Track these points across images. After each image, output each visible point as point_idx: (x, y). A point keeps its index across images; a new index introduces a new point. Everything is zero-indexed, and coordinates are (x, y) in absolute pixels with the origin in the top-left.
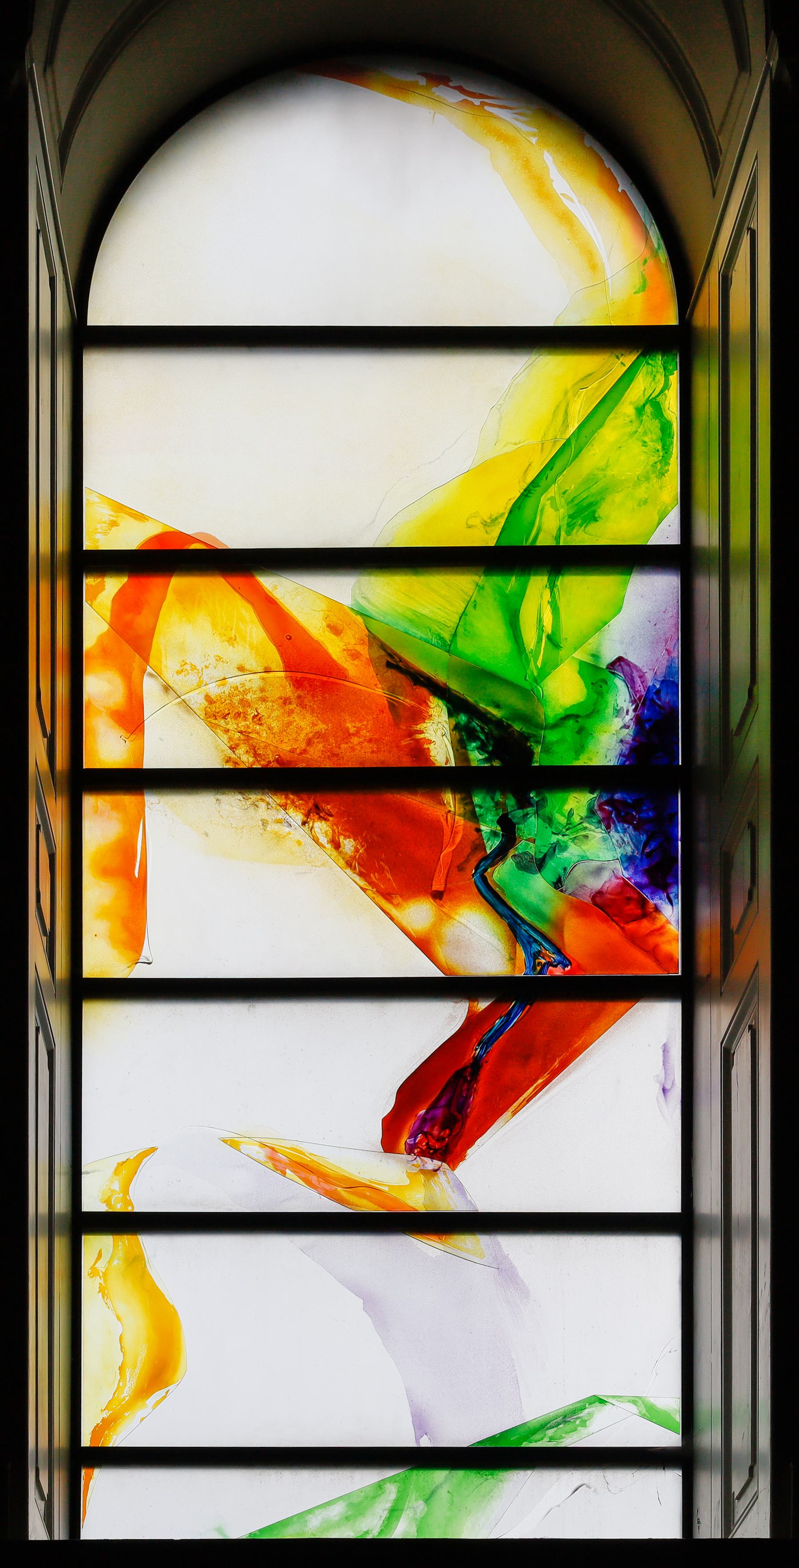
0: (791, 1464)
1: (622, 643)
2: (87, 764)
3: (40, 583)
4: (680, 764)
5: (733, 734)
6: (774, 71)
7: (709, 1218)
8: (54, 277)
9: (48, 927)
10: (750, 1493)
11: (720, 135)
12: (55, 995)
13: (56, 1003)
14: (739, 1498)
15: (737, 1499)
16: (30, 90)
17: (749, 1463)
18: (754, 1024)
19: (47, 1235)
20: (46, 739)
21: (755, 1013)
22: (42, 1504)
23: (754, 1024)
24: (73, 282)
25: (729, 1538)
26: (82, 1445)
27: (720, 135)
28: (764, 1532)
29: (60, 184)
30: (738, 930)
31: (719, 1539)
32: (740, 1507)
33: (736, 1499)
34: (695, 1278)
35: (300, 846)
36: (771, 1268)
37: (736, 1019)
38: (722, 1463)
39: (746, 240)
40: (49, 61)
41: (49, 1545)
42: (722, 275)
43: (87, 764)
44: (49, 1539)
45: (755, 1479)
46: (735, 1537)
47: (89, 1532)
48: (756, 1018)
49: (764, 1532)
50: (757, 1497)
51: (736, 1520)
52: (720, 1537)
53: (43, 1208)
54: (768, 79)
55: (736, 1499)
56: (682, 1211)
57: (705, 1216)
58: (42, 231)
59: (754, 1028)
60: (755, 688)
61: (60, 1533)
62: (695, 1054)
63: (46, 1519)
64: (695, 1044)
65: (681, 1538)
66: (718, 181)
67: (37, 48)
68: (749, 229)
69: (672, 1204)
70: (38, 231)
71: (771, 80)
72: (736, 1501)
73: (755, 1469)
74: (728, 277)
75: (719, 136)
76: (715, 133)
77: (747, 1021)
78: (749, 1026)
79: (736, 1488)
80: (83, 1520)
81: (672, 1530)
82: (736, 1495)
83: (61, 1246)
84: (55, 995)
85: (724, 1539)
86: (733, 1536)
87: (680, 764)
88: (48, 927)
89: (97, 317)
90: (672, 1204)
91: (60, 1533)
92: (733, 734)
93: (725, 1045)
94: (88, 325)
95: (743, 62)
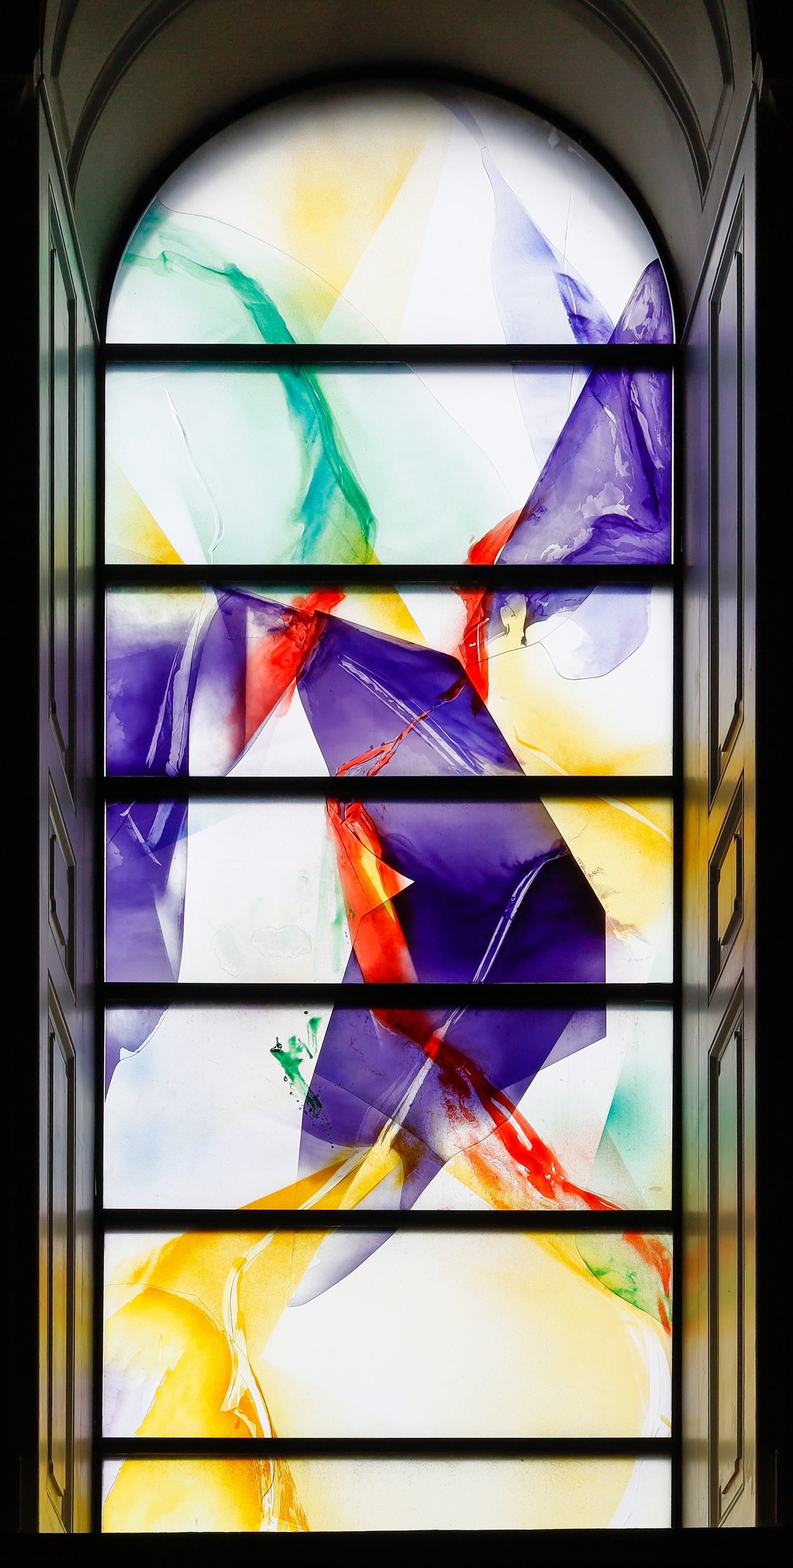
0: (776, 1450)
2: (106, 1434)
4: (672, 563)
5: (721, 943)
8: (74, 300)
11: (710, 150)
12: (76, 813)
13: (77, 1012)
18: (739, 1030)
25: (719, 1527)
27: (710, 150)
28: (751, 1523)
30: (726, 748)
31: (707, 1528)
32: (726, 1502)
34: (683, 1110)
35: (312, 1058)
36: (756, 645)
37: (724, 1024)
38: (709, 562)
39: (733, 845)
43: (106, 1434)
44: (66, 1532)
46: (722, 1527)
47: (112, 1524)
48: (742, 1026)
49: (751, 1523)
50: (743, 1489)
51: (723, 1510)
52: (708, 1527)
53: (59, 1433)
58: (57, 249)
61: (80, 1525)
63: (67, 967)
64: (683, 970)
65: (671, 1528)
66: (706, 199)
68: (736, 836)
74: (717, 867)
75: (709, 152)
76: (705, 147)
77: (734, 1027)
78: (735, 1032)
79: (723, 1481)
80: (106, 1094)
81: (664, 1522)
83: (82, 1245)
84: (76, 813)
85: (711, 1528)
87: (672, 563)
89: (114, 336)
90: (664, 1203)
92: (721, 943)
93: (711, 1054)
95: (728, 76)
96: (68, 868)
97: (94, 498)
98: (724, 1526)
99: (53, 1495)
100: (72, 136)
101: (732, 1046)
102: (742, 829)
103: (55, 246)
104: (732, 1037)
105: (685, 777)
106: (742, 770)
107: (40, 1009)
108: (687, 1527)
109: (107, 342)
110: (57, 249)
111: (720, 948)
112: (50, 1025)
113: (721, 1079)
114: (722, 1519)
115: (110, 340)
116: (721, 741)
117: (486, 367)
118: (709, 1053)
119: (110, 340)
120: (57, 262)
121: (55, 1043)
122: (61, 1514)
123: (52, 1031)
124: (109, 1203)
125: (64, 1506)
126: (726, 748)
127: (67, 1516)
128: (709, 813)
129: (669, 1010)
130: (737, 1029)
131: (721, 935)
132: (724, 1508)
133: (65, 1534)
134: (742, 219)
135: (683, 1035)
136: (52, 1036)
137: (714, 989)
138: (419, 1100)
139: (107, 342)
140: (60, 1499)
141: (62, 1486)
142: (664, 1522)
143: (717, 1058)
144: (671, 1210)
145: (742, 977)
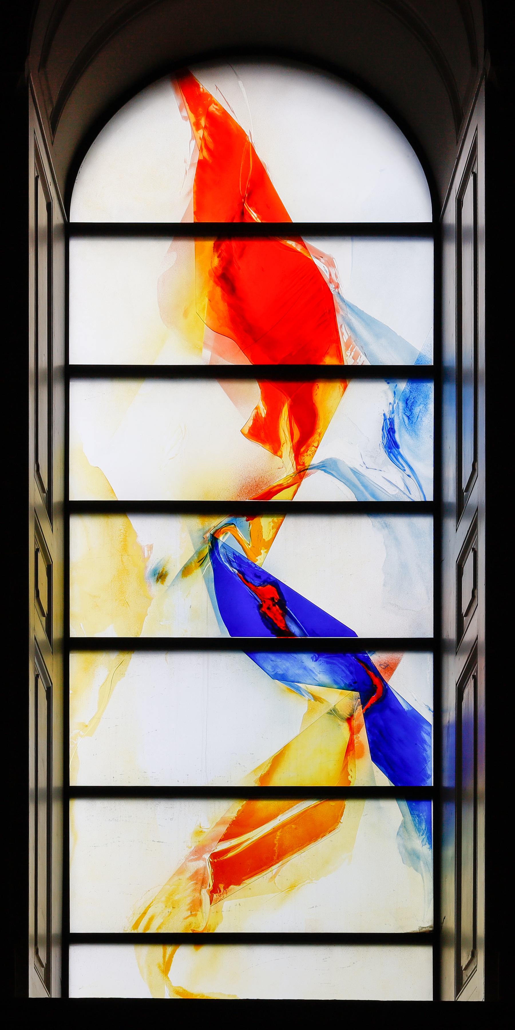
1: (403, 436)
2: (72, 931)
3: (39, 246)
5: (464, 491)
6: (488, 74)
7: (450, 504)
8: (51, 203)
10: (472, 967)
14: (466, 969)
15: (464, 970)
16: (30, 91)
18: (475, 674)
19: (46, 801)
20: (45, 618)
26: (71, 932)
29: (51, 140)
32: (466, 974)
33: (465, 492)
39: (471, 555)
40: (43, 64)
42: (458, 564)
43: (72, 931)
45: (475, 960)
46: (458, 1000)
47: (75, 992)
50: (477, 970)
51: (464, 982)
53: (43, 783)
54: (484, 81)
55: (465, 492)
60: (476, 464)
61: (55, 993)
67: (33, 61)
68: (473, 549)
69: (429, 633)
78: (473, 675)
79: (464, 963)
81: (428, 996)
89: (76, 217)
90: (429, 633)
91: (55, 993)
92: (464, 491)
96: (47, 566)
97: (64, 451)
99: (38, 965)
100: (55, 99)
101: (471, 683)
102: (477, 544)
107: (29, 944)
108: (444, 1000)
109: (70, 785)
112: (35, 670)
116: (464, 486)
117: (317, 237)
118: (456, 685)
120: (40, 185)
121: (39, 680)
123: (37, 673)
124: (74, 633)
128: (457, 530)
130: (474, 546)
132: (465, 978)
134: (476, 528)
136: (37, 677)
137: (459, 645)
140: (43, 969)
141: (44, 961)
142: (428, 996)
143: (462, 566)
144: (433, 500)
145: (477, 513)
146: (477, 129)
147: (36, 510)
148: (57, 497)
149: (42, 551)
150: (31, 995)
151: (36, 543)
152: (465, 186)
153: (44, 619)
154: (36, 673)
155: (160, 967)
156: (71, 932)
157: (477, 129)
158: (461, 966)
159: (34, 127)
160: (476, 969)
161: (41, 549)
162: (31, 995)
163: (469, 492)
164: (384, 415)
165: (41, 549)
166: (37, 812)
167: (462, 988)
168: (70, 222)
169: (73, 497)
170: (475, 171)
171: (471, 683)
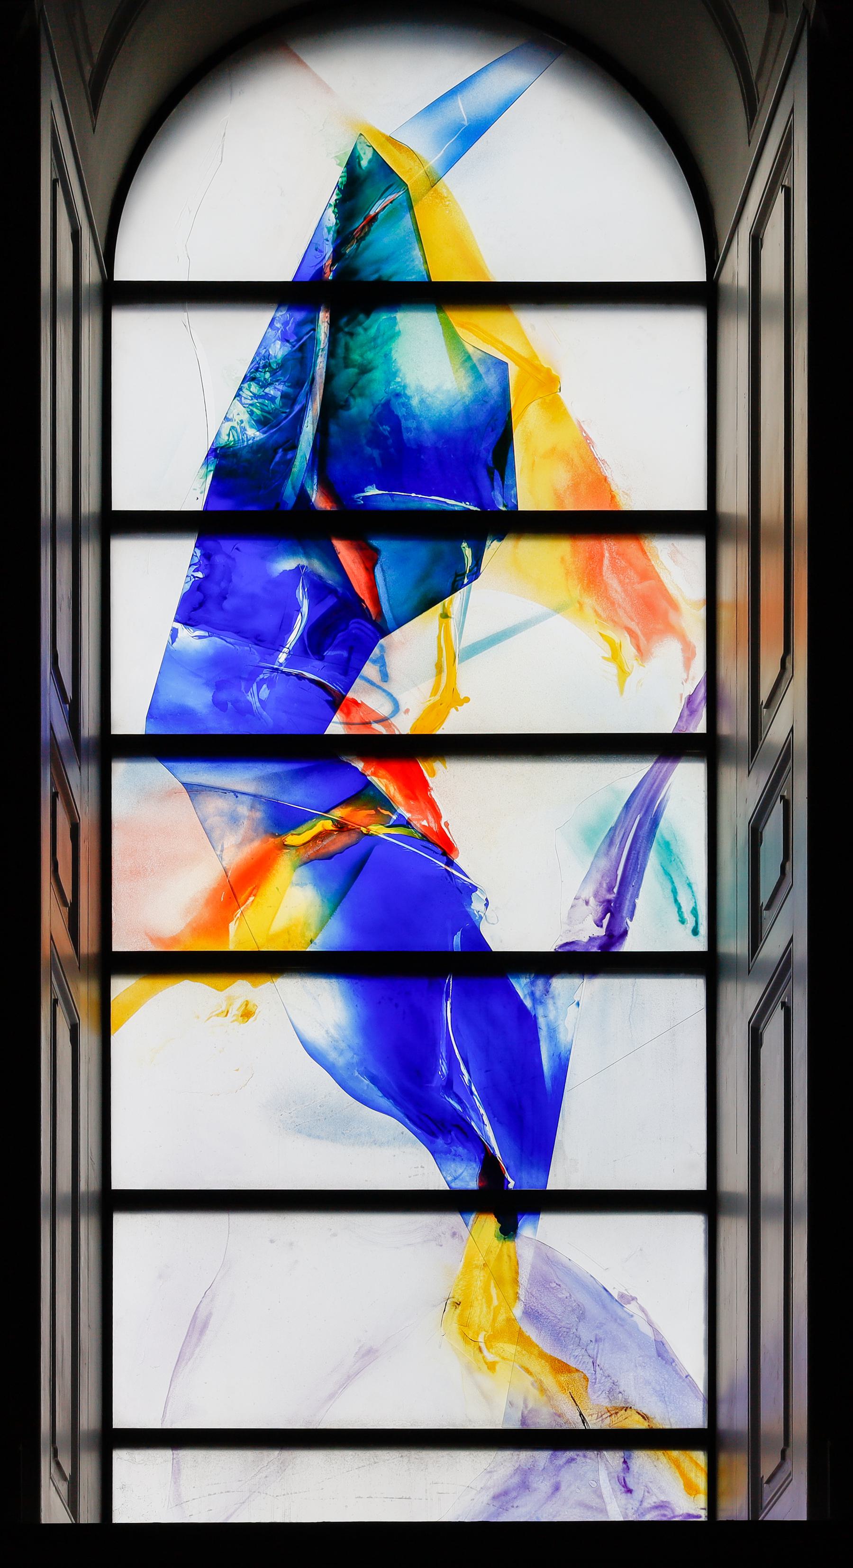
6: (812, 17)
9: (69, 694)
12: (79, 968)
14: (769, 907)
17: (781, 1445)
18: (786, 1000)
21: (791, 125)
22: (64, 1487)
23: (786, 1000)
24: (104, 249)
25: (760, 1519)
28: (802, 1515)
30: (769, 704)
32: (768, 1492)
34: (718, 1134)
41: (74, 1530)
44: (74, 1522)
46: (766, 1519)
47: (120, 1516)
48: (791, 996)
49: (802, 1515)
50: (792, 1480)
51: (764, 1504)
55: (764, 708)
56: (707, 1187)
57: (728, 516)
58: (60, 180)
59: (786, 798)
61: (88, 1515)
62: (717, 1293)
68: (782, 797)
69: (697, 1182)
70: (54, 183)
71: (808, 27)
72: (765, 710)
73: (788, 1452)
74: (758, 830)
78: (781, 796)
82: (765, 1480)
84: (79, 968)
85: (751, 1521)
86: (764, 1517)
88: (69, 694)
94: (115, 280)
96: (71, 1026)
97: (100, 1052)
98: (768, 1518)
99: (56, 1477)
103: (58, 175)
104: (777, 803)
105: (718, 1190)
106: (791, 108)
109: (112, 1188)
110: (60, 180)
111: (762, 1487)
112: (52, 784)
113: (764, 1052)
114: (764, 1511)
115: (117, 947)
116: (764, 696)
119: (117, 947)
122: (66, 1498)
123: (54, 996)
125: (70, 1492)
126: (769, 704)
127: (73, 1504)
129: (702, 761)
130: (785, 183)
131: (764, 899)
133: (72, 1524)
135: (717, 1145)
136: (54, 796)
138: (417, 1460)
139: (113, 950)
141: (68, 1471)
146: (792, 111)
147: (54, 937)
148: (89, 727)
149: (63, 1006)
150: (45, 1520)
151: (55, 964)
152: (762, 228)
153: (66, 910)
154: (53, 997)
155: (604, 461)
156: (114, 1427)
157: (792, 111)
158: (761, 1476)
159: (50, 97)
160: (791, 1477)
161: (60, 1001)
162: (45, 1520)
163: (771, 709)
164: (603, 657)
165: (60, 1001)
166: (55, 483)
167: (762, 1514)
168: (116, 279)
169: (119, 503)
170: (786, 184)
171: (778, 1016)
